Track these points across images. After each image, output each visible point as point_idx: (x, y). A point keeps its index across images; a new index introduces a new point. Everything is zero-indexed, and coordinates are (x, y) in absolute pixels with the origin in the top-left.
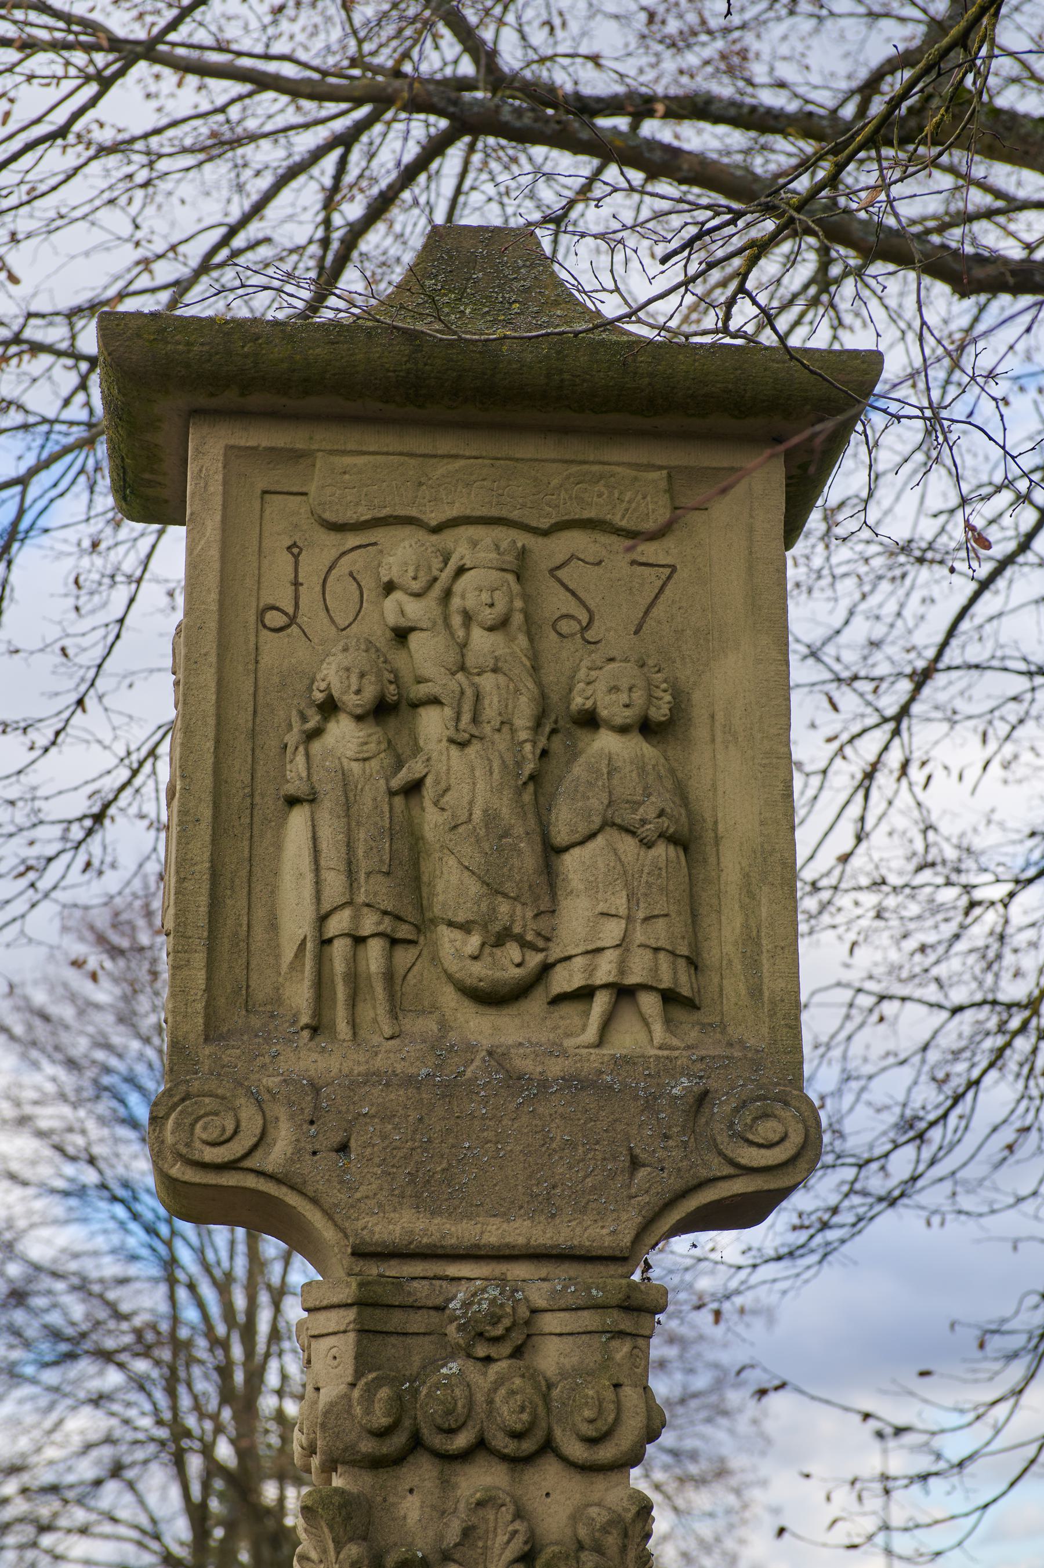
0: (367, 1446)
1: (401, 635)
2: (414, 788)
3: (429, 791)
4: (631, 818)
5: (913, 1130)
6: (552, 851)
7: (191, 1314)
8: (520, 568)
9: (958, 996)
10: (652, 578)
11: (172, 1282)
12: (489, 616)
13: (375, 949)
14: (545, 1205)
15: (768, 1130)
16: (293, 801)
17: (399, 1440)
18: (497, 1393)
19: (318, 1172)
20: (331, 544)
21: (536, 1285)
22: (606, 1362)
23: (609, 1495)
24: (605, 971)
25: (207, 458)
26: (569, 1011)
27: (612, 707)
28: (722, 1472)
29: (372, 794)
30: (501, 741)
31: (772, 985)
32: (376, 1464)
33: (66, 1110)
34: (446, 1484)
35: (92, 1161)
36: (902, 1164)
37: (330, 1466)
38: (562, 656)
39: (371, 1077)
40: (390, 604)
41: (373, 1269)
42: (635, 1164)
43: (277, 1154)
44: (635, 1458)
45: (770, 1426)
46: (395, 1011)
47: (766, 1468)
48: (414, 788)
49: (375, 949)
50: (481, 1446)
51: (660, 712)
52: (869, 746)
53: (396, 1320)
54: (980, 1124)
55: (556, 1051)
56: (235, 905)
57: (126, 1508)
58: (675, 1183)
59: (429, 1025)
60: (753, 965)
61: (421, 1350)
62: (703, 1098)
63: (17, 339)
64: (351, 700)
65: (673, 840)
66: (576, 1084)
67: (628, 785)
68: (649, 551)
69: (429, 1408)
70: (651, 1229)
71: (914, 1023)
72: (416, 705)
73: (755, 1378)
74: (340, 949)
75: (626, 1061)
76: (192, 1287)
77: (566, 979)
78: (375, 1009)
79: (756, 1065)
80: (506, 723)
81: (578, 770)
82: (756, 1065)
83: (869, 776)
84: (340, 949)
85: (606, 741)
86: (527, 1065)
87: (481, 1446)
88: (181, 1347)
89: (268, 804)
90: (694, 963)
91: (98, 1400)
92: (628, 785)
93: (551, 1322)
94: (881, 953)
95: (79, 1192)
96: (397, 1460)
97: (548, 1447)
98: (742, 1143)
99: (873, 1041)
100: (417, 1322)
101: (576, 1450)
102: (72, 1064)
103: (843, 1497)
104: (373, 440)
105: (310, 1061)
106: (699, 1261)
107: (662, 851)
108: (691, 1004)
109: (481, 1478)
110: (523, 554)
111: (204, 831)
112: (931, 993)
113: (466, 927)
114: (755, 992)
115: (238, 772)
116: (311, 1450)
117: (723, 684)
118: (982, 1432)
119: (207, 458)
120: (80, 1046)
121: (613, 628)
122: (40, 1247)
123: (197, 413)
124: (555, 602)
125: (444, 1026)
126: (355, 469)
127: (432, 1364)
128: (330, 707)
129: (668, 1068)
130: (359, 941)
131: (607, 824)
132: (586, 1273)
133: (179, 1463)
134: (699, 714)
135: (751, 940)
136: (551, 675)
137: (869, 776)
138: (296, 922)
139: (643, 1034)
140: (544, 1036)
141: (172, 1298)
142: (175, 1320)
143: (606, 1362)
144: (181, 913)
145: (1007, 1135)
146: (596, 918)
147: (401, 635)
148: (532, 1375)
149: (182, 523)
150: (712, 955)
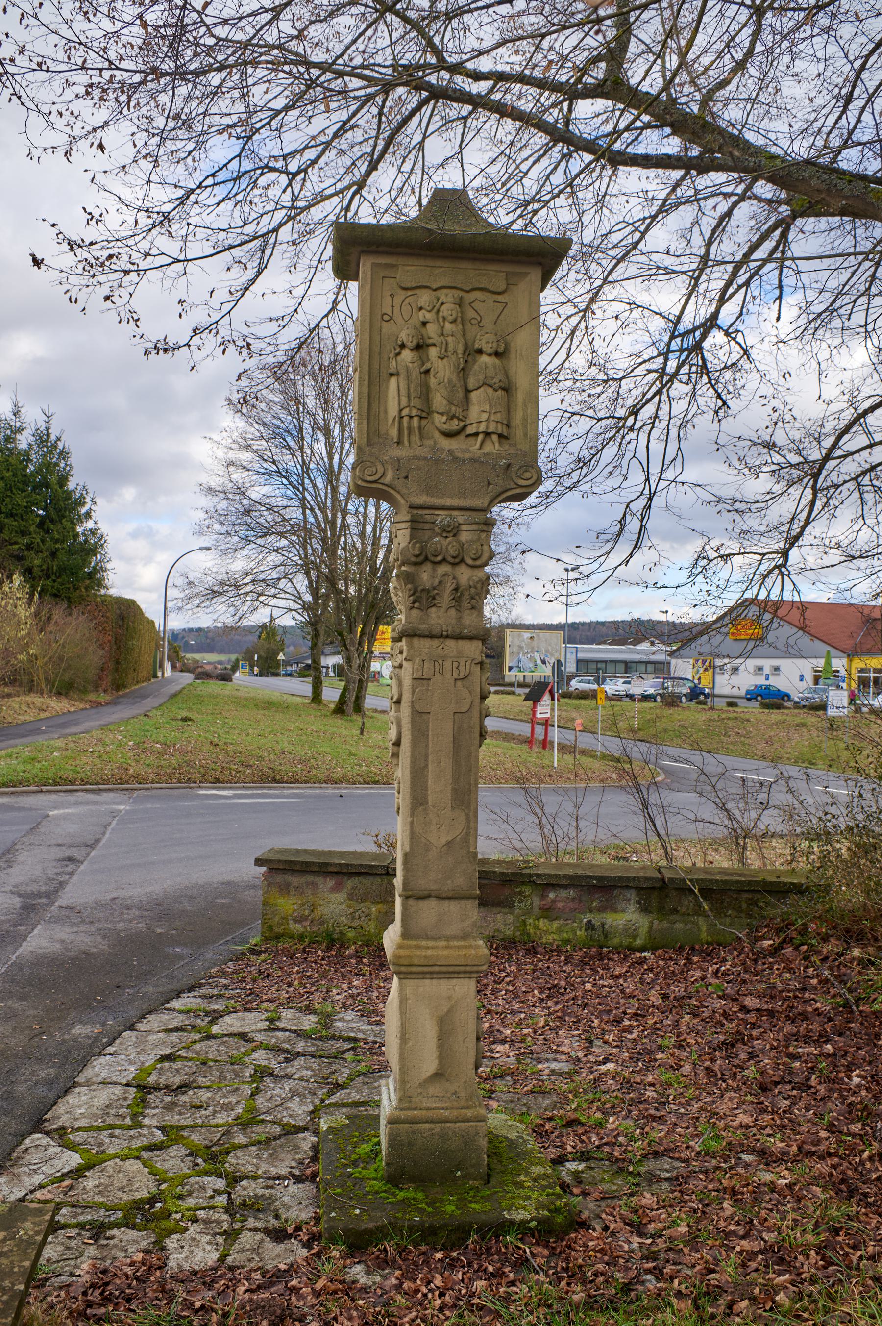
0: (413, 559)
1: (424, 324)
2: (427, 371)
3: (432, 373)
4: (492, 382)
5: (581, 462)
6: (468, 391)
7: (312, 520)
8: (460, 303)
9: (601, 414)
10: (500, 306)
11: (304, 508)
12: (451, 318)
13: (416, 420)
14: (463, 495)
15: (527, 475)
16: (392, 375)
17: (422, 558)
18: (449, 546)
19: (399, 484)
20: (403, 294)
21: (460, 517)
22: (479, 539)
23: (479, 574)
24: (482, 428)
25: (366, 265)
26: (471, 439)
27: (487, 348)
28: (508, 580)
29: (415, 373)
30: (454, 358)
31: (530, 433)
32: (415, 564)
33: (264, 442)
34: (434, 570)
35: (274, 462)
36: (575, 476)
37: (403, 564)
38: (472, 331)
39: (415, 457)
40: (421, 313)
41: (415, 512)
42: (489, 484)
43: (388, 479)
44: (486, 564)
45: (525, 565)
46: (421, 437)
47: (523, 580)
48: (427, 371)
49: (416, 420)
50: (444, 560)
51: (501, 350)
52: (574, 320)
53: (421, 526)
54: (602, 464)
55: (467, 451)
56: (375, 406)
57: (289, 587)
58: (500, 489)
59: (431, 442)
60: (525, 427)
61: (428, 534)
62: (509, 465)
63: (267, 166)
64: (409, 344)
65: (504, 389)
66: (474, 460)
67: (491, 372)
68: (500, 298)
69: (430, 549)
70: (491, 503)
71: (584, 424)
72: (428, 346)
73: (521, 548)
74: (406, 420)
75: (488, 454)
76: (312, 510)
77: (471, 430)
78: (416, 437)
79: (525, 456)
80: (455, 352)
81: (476, 367)
82: (525, 456)
83: (573, 333)
84: (406, 420)
85: (484, 358)
86: (459, 455)
87: (444, 560)
88: (308, 532)
89: (385, 375)
90: (508, 426)
91: (277, 550)
92: (491, 372)
93: (464, 527)
94: (572, 401)
95: (269, 474)
96: (421, 563)
97: (462, 561)
98: (518, 476)
99: (567, 432)
100: (427, 526)
101: (470, 562)
102: (264, 424)
103: (549, 586)
104: (417, 262)
105: (397, 452)
106: (504, 511)
107: (500, 392)
108: (506, 438)
109: (443, 569)
110: (461, 298)
111: (366, 383)
112: (590, 413)
113: (442, 414)
114: (526, 435)
115: (376, 366)
116: (396, 560)
117: (520, 340)
118: (596, 565)
119: (366, 265)
120: (268, 418)
121: (487, 322)
122: (255, 493)
123: (363, 252)
124: (471, 314)
125: (435, 443)
126: (411, 270)
127: (431, 538)
128: (403, 346)
129: (499, 457)
130: (411, 417)
131: (484, 384)
132: (474, 514)
133: (307, 573)
134: (513, 350)
135: (525, 420)
136: (469, 336)
137: (573, 333)
138: (393, 411)
139: (492, 447)
140: (464, 446)
141: (304, 513)
142: (305, 521)
143: (479, 539)
144: (360, 408)
145: (610, 468)
146: (480, 411)
147: (424, 324)
148: (459, 542)
149: (356, 279)
150: (513, 424)
